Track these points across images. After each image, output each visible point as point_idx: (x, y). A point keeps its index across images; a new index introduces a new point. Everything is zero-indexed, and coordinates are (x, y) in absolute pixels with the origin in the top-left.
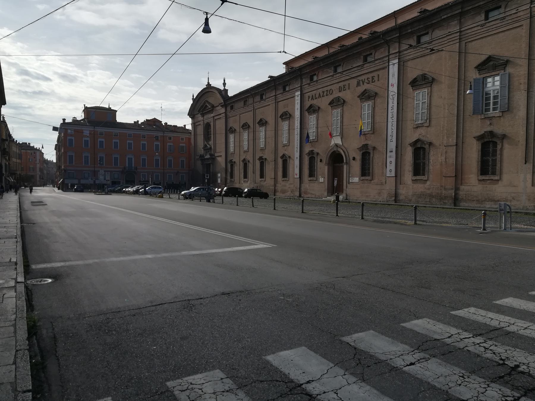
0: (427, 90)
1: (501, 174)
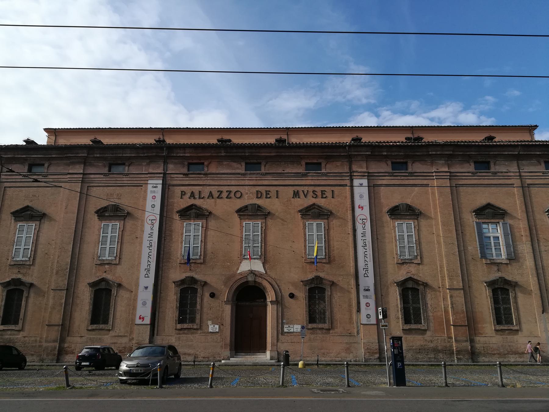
0: (34, 225)
1: (519, 323)
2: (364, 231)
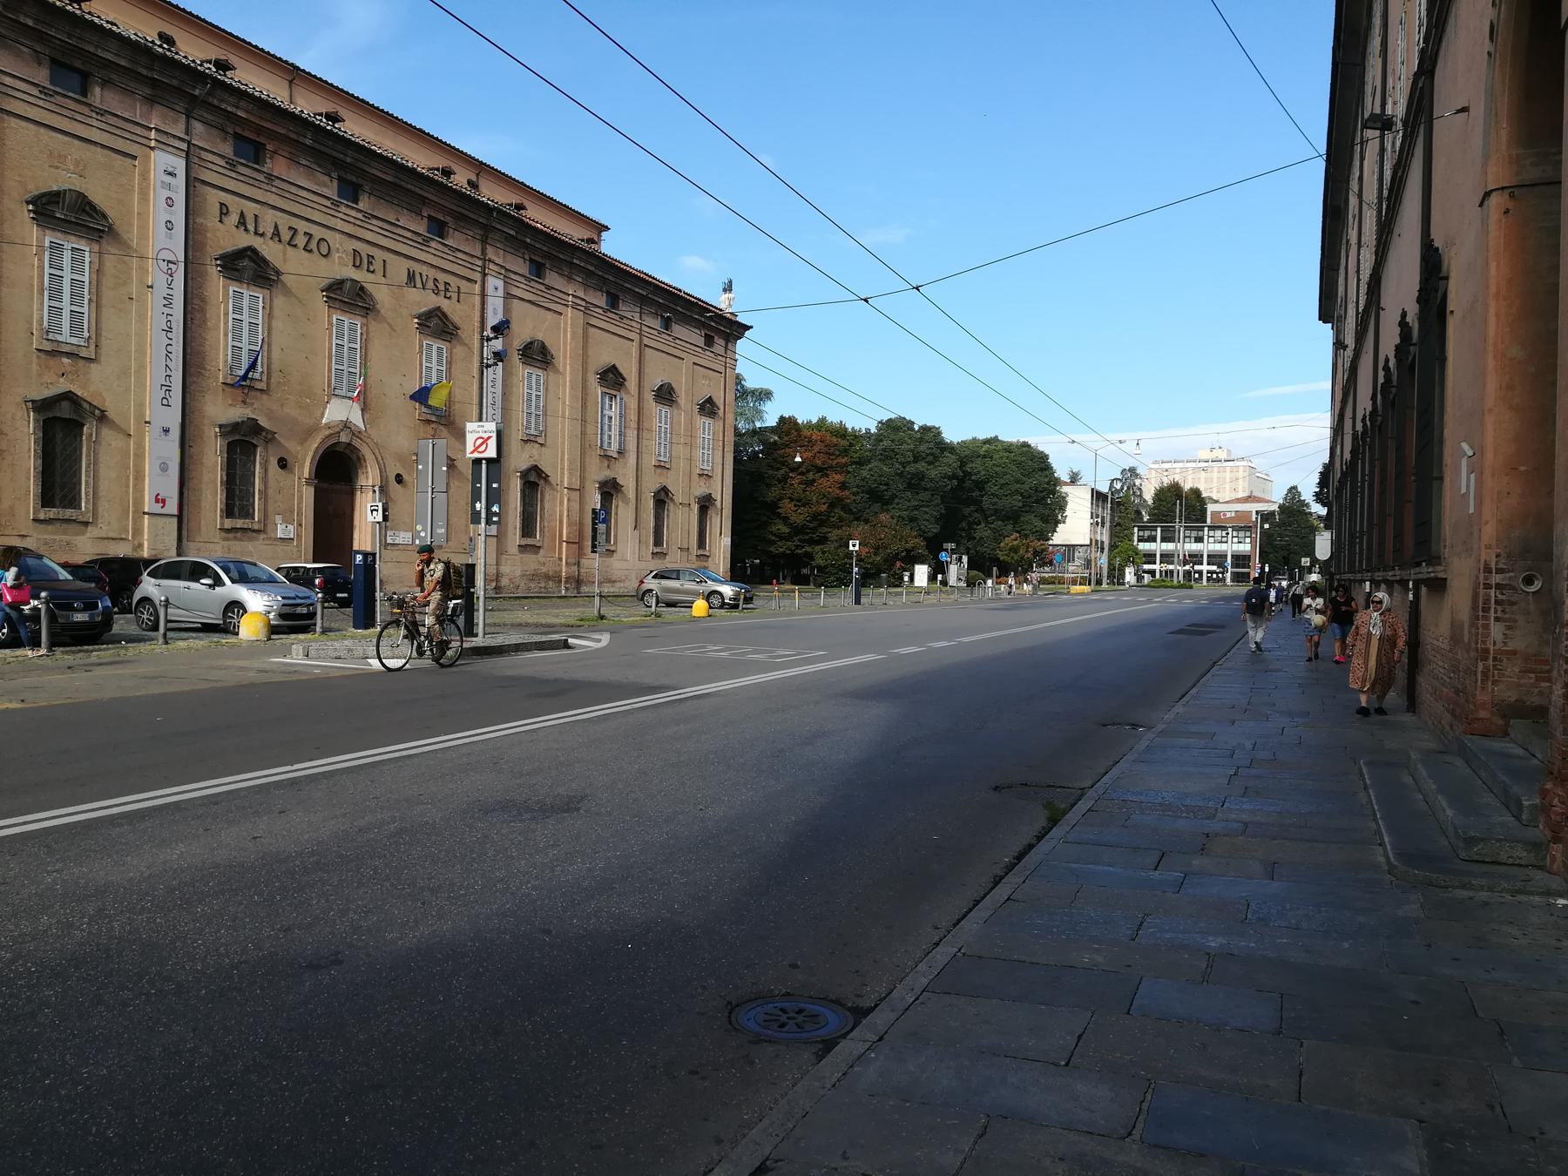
2: (170, 292)
